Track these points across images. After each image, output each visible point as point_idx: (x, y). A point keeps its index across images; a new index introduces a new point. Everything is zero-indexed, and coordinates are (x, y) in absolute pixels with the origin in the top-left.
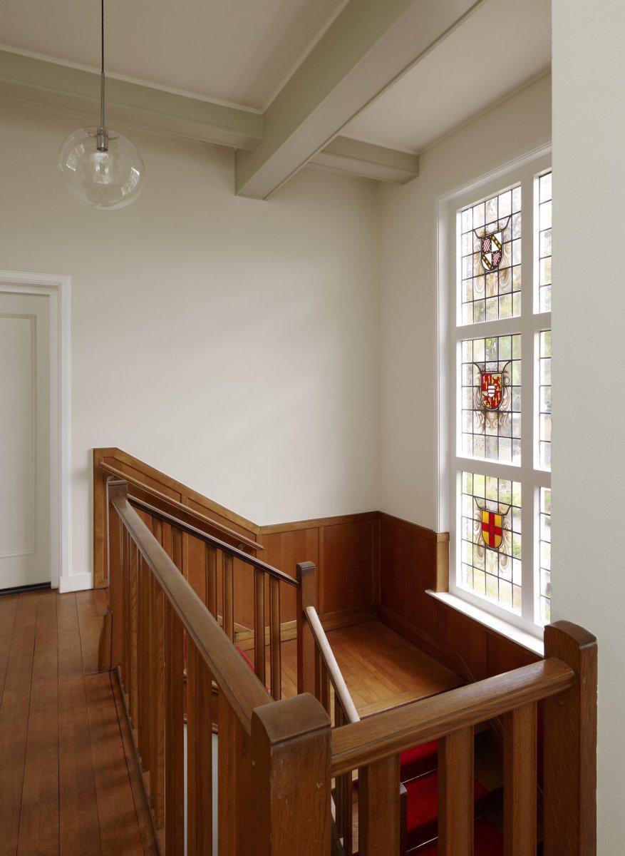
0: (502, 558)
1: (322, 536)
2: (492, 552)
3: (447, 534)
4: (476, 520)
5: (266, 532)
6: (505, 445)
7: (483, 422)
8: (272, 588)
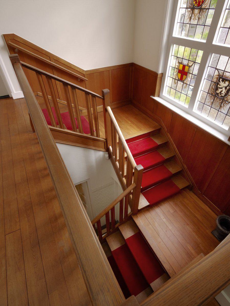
0: (185, 85)
1: (110, 73)
2: (181, 82)
3: (162, 74)
4: (176, 68)
5: (88, 73)
6: (199, 29)
7: (190, 16)
8: (93, 101)
